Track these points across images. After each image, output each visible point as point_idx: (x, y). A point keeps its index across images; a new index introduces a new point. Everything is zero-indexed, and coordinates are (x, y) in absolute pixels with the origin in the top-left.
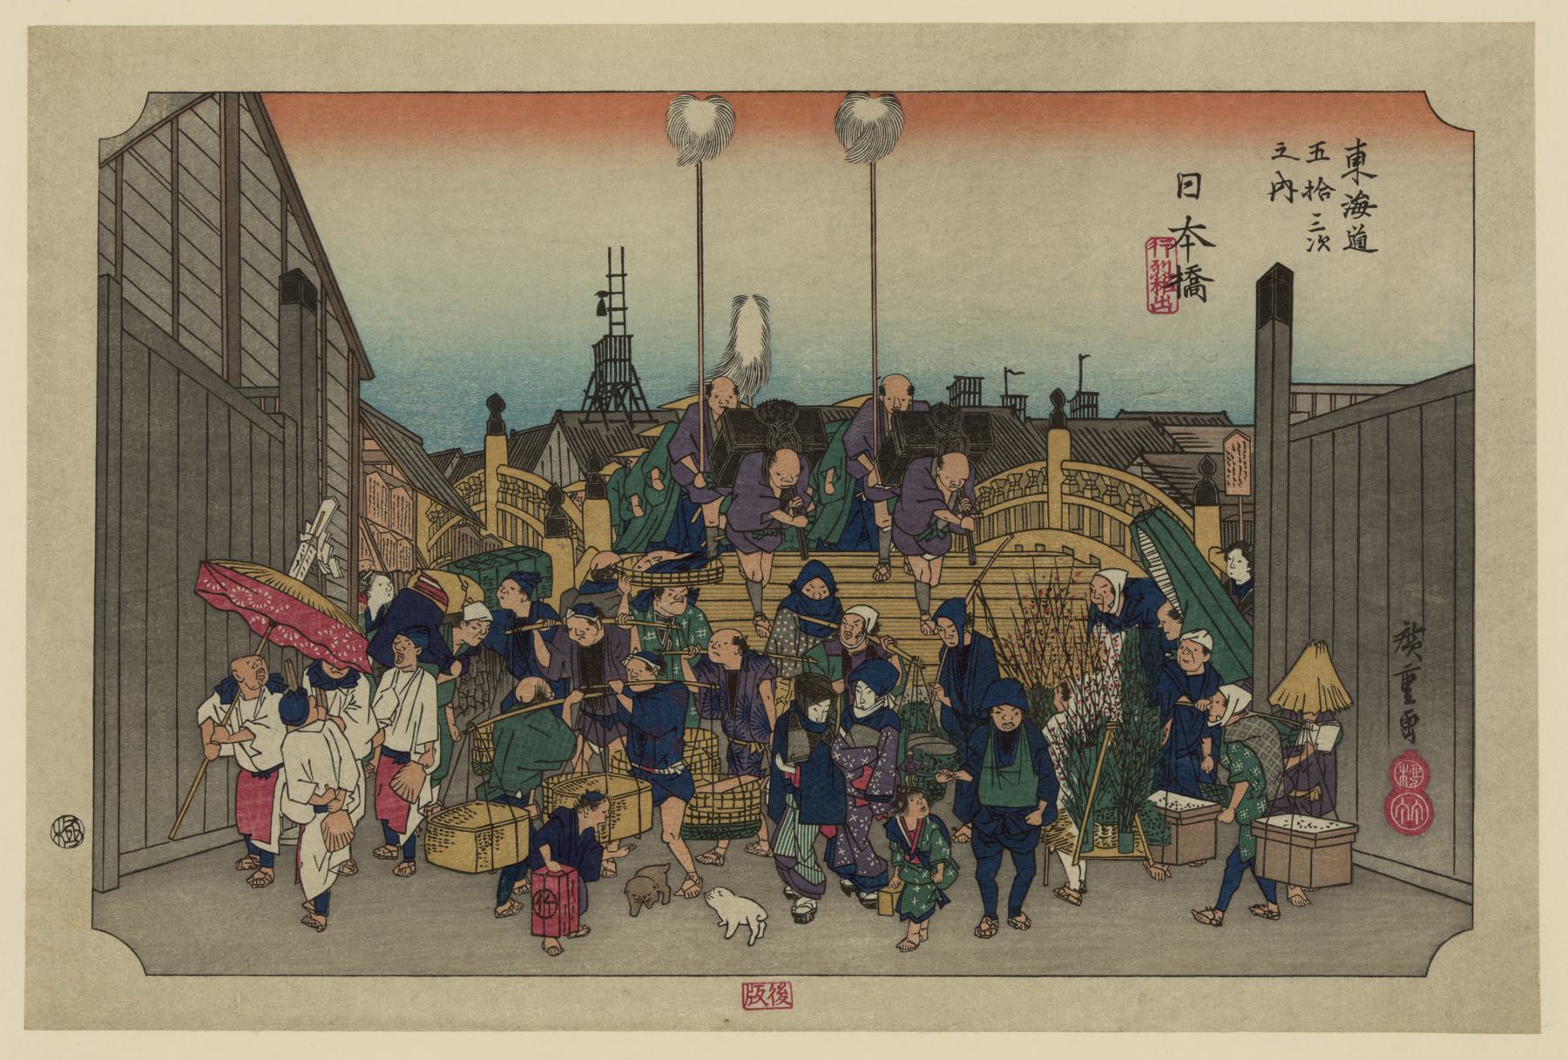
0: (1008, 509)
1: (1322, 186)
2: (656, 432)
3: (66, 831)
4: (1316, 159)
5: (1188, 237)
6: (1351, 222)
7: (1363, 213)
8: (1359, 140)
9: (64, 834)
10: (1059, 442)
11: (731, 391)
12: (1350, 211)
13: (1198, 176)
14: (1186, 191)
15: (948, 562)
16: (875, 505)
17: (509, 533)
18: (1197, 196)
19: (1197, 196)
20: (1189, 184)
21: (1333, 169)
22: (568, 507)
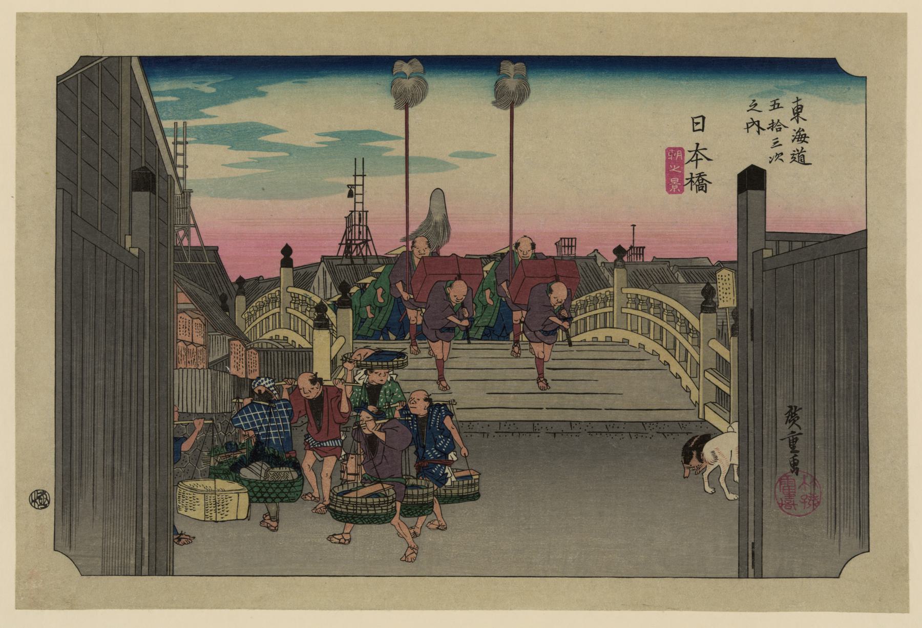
0: (597, 314)
1: (779, 124)
2: (380, 270)
3: (38, 499)
4: (774, 109)
5: (697, 155)
6: (798, 146)
7: (804, 141)
8: (797, 98)
9: (38, 501)
10: (619, 276)
11: (530, 247)
12: (796, 140)
13: (704, 118)
14: (697, 127)
15: (556, 348)
16: (514, 312)
17: (292, 325)
18: (703, 130)
19: (703, 130)
20: (698, 123)
21: (785, 115)
22: (330, 313)
